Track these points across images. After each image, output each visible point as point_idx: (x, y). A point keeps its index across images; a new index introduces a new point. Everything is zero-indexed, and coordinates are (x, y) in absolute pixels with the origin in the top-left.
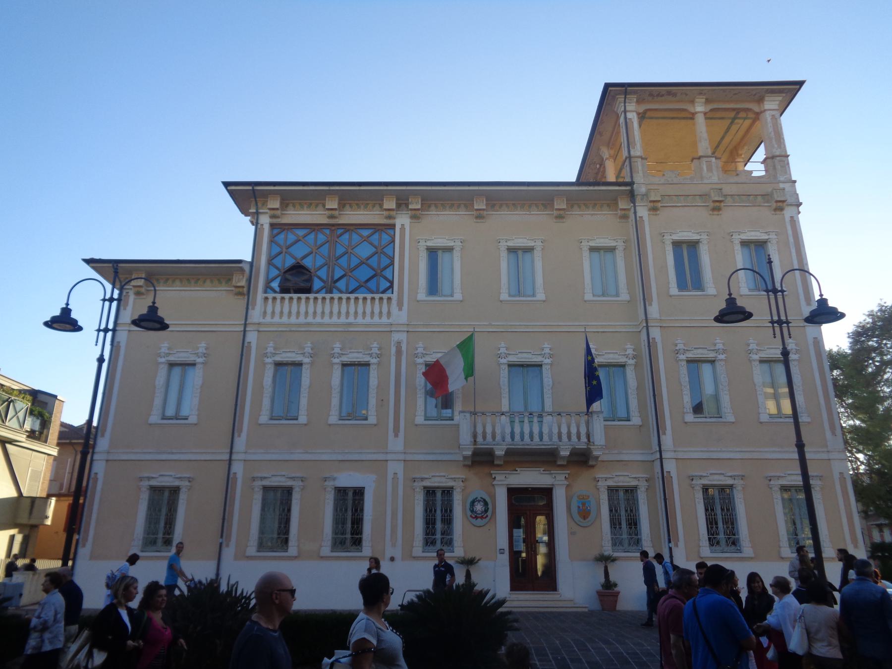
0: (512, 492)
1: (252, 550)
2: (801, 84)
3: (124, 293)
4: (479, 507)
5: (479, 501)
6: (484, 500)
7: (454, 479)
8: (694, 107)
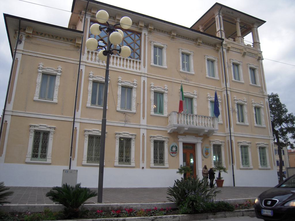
0: (184, 144)
1: (85, 162)
2: (265, 22)
3: (20, 36)
4: (174, 149)
5: (174, 147)
6: (176, 147)
7: (165, 138)
8: (237, 20)
